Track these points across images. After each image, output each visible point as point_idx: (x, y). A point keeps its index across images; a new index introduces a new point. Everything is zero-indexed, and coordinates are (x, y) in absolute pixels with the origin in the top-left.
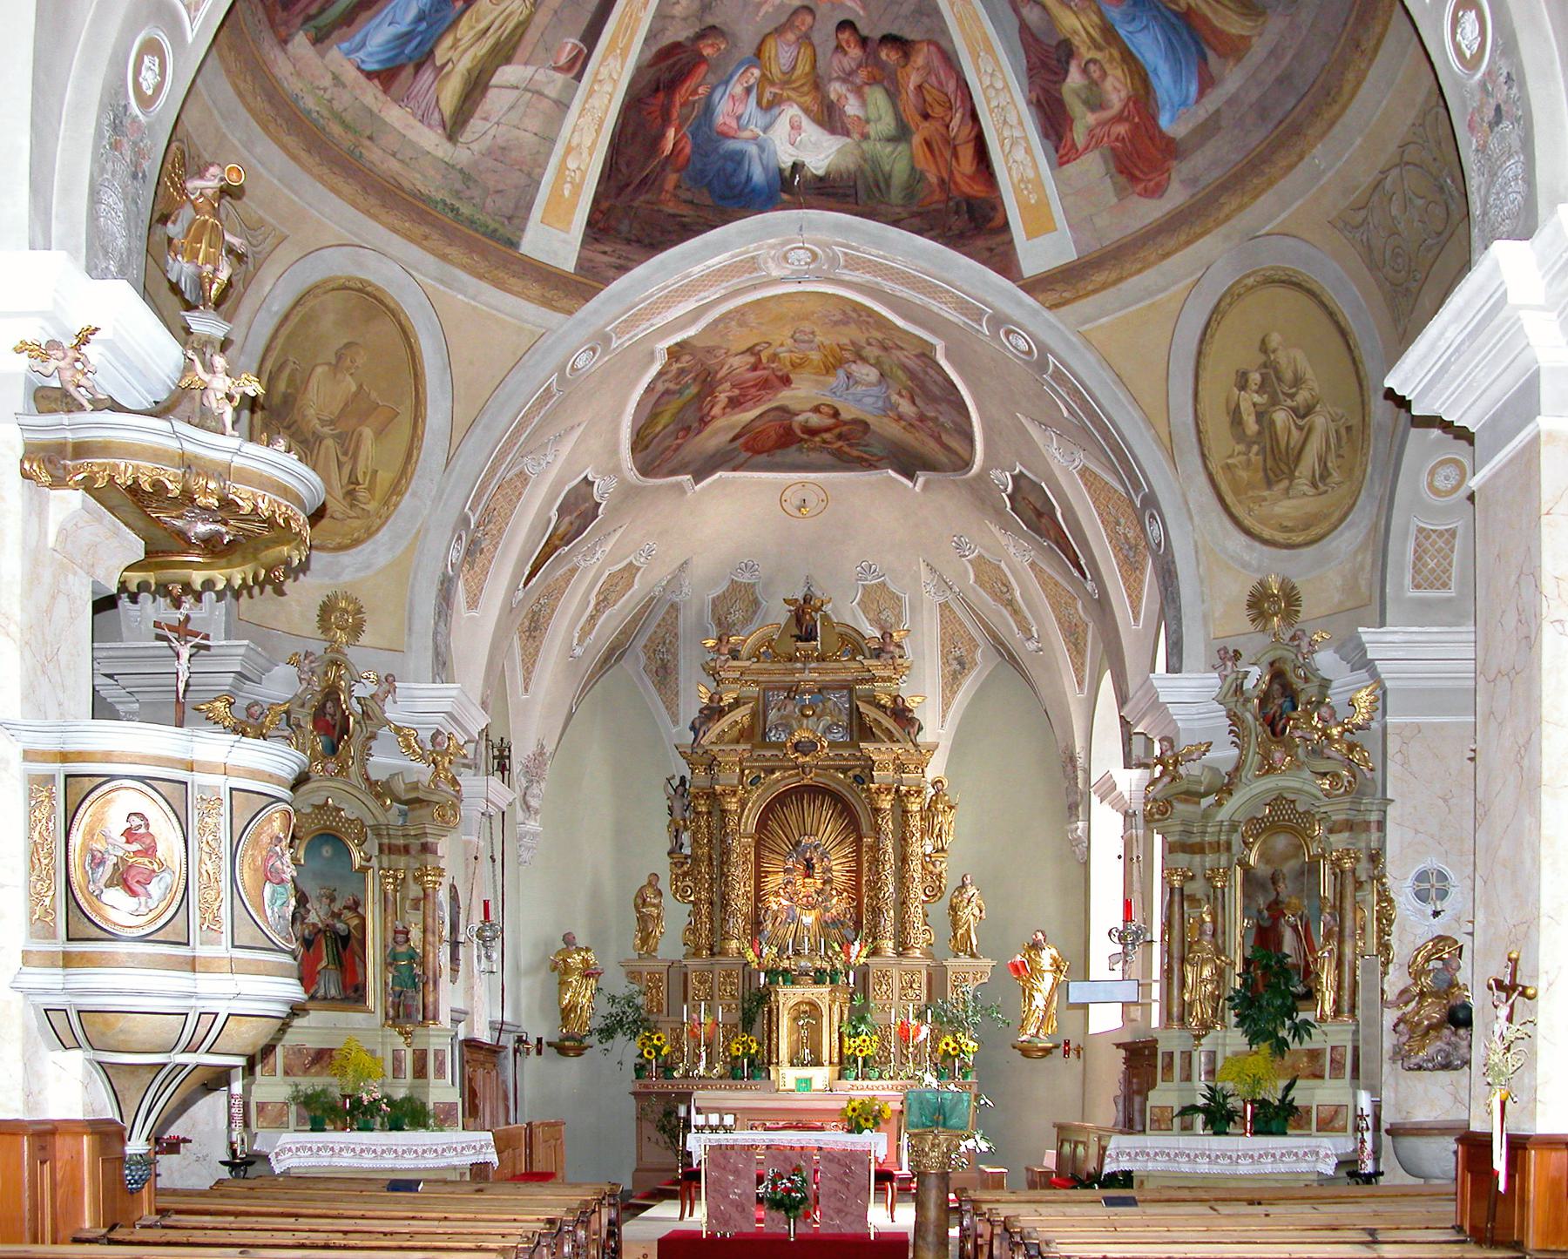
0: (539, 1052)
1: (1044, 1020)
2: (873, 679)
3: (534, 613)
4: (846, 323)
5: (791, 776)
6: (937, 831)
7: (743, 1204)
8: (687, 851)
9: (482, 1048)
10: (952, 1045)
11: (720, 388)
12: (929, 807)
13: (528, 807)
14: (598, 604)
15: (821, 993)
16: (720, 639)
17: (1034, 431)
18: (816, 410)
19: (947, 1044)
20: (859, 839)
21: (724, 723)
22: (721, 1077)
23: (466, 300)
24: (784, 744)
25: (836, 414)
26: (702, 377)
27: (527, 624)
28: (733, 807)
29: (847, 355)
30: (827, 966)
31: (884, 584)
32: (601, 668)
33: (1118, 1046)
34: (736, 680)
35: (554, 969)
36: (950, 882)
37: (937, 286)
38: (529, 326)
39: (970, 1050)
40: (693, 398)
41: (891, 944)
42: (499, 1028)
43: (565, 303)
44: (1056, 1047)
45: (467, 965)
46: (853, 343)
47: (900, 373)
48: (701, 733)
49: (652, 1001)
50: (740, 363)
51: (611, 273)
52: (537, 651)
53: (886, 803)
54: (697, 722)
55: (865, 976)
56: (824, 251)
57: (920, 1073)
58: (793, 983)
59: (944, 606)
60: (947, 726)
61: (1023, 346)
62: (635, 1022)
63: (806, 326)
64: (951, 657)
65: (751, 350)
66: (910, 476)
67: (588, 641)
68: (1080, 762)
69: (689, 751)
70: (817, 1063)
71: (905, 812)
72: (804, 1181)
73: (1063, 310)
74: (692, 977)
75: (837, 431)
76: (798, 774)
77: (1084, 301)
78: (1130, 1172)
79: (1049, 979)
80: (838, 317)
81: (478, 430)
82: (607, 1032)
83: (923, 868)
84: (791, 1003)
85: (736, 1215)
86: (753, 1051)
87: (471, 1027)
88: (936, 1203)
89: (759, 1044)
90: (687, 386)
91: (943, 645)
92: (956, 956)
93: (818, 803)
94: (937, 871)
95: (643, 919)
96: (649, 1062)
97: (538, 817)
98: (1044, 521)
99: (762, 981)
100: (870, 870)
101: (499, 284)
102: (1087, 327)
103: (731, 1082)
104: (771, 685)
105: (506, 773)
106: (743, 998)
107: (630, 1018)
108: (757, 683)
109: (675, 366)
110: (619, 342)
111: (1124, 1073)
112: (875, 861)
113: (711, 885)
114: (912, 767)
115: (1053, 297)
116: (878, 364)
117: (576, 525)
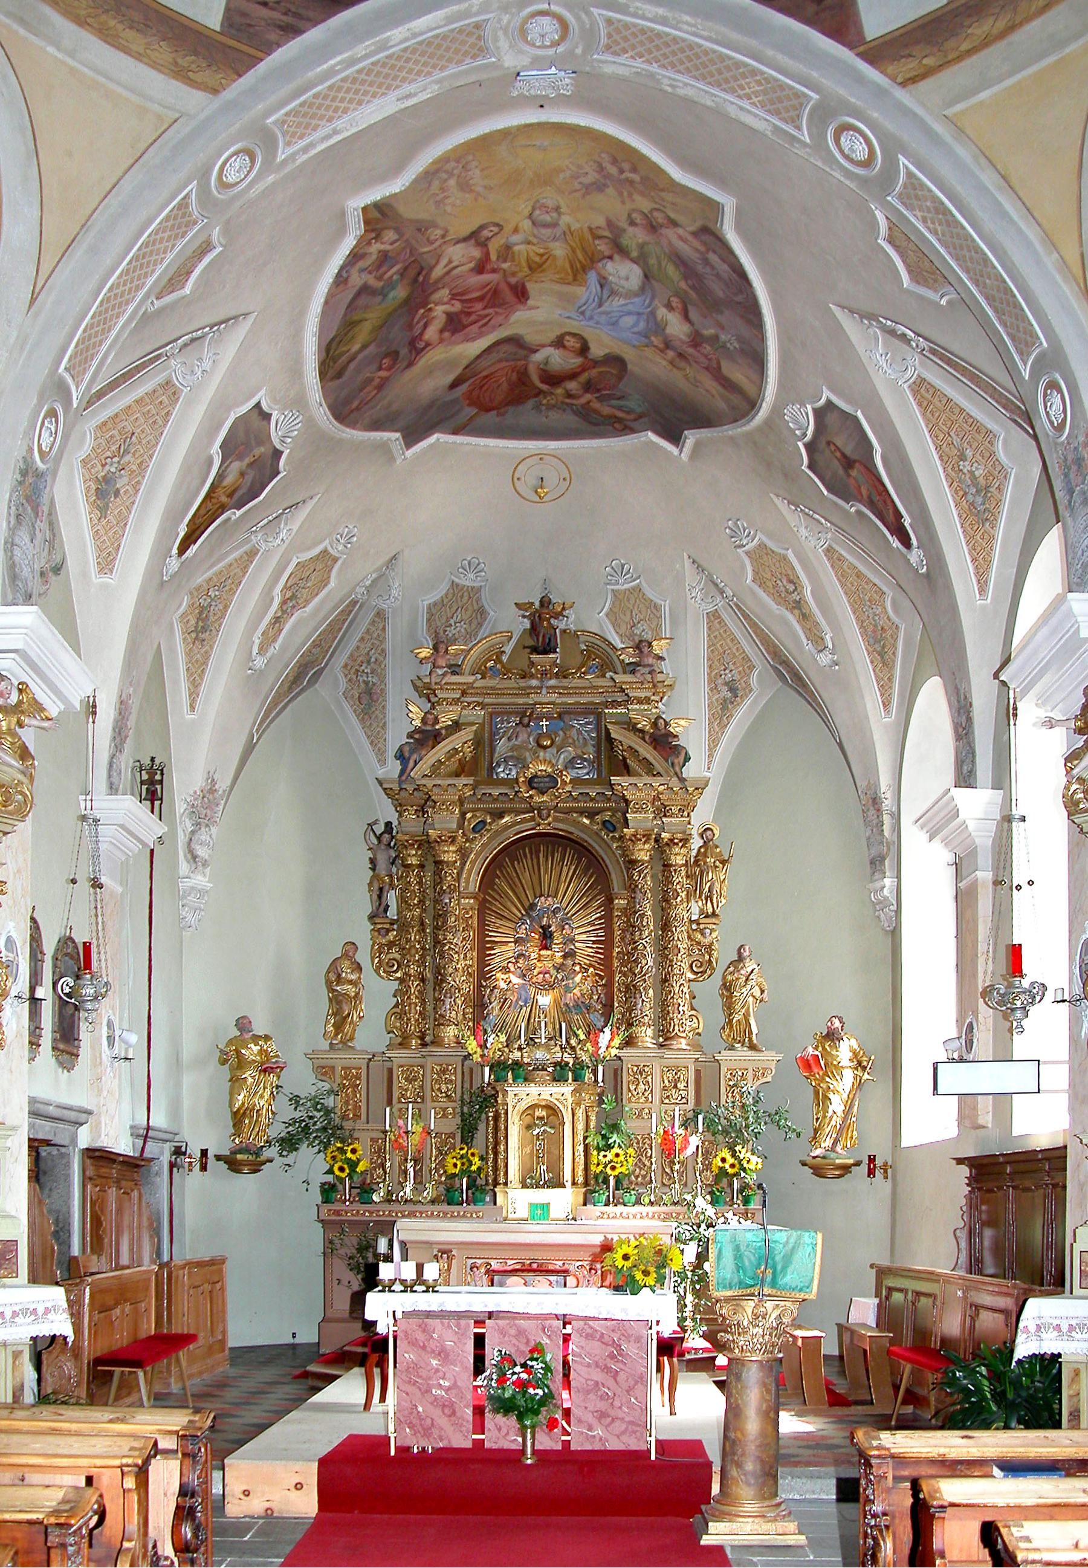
0: (204, 1168)
1: (842, 1129)
2: (628, 700)
3: (202, 609)
4: (600, 187)
5: (524, 821)
7: (452, 1403)
8: (392, 913)
9: (114, 1161)
10: (730, 1160)
11: (436, 296)
12: (696, 862)
13: (194, 857)
15: (562, 1093)
16: (436, 648)
17: (850, 326)
18: (559, 343)
19: (723, 1160)
20: (610, 900)
21: (440, 751)
22: (433, 1202)
23: (60, 56)
24: (516, 780)
25: (584, 349)
26: (412, 273)
27: (193, 622)
29: (603, 247)
30: (569, 1059)
31: (638, 589)
32: (290, 689)
33: (960, 1161)
34: (456, 701)
35: (223, 1062)
36: (723, 955)
37: (738, 64)
38: (156, 108)
39: (752, 1166)
40: (401, 306)
41: (650, 1032)
42: (146, 1134)
43: (205, 76)
44: (858, 1164)
45: (93, 1048)
46: (610, 224)
47: (671, 270)
49: (347, 1103)
50: (461, 255)
51: (273, 36)
52: (207, 656)
53: (643, 852)
54: (406, 749)
55: (617, 1074)
56: (578, 18)
57: (688, 1197)
58: (526, 1080)
59: (714, 617)
60: (714, 767)
61: (860, 152)
62: (324, 1129)
63: (550, 197)
64: (720, 681)
65: (474, 237)
66: (675, 438)
67: (271, 651)
68: (887, 804)
69: (396, 787)
70: (557, 1183)
71: (667, 866)
72: (547, 1368)
73: (923, 85)
74: (397, 1072)
75: (585, 377)
76: (533, 819)
77: (955, 68)
78: (1055, 1358)
79: (848, 1076)
80: (592, 176)
81: (79, 252)
82: (289, 1144)
83: (689, 937)
84: (523, 1105)
85: (443, 1421)
86: (474, 1168)
87: (96, 1131)
88: (759, 1410)
89: (482, 1158)
90: (391, 285)
91: (710, 667)
92: (732, 1048)
93: (557, 856)
94: (707, 941)
95: (337, 1000)
96: (342, 1181)
97: (208, 870)
98: (854, 473)
99: (486, 1080)
100: (623, 939)
101: (105, 35)
102: (958, 107)
103: (445, 1207)
104: (499, 709)
105: (157, 803)
106: (462, 1100)
107: (319, 1125)
108: (483, 706)
109: (375, 248)
110: (290, 150)
111: (969, 1198)
112: (632, 927)
113: (423, 956)
114: (675, 810)
115: (908, 67)
116: (641, 260)
117: (249, 478)
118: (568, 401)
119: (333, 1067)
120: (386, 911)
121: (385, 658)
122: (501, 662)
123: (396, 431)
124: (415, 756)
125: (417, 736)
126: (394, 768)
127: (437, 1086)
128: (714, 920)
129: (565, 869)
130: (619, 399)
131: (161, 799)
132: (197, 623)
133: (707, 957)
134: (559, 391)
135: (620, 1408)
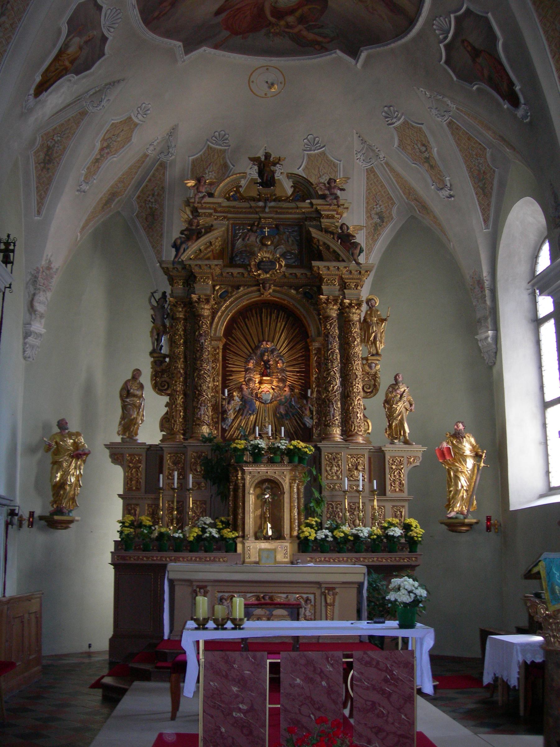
3: (49, 148)
6: (372, 338)
14: (102, 149)
28: (206, 313)
36: (385, 382)
48: (182, 250)
52: (50, 180)
59: (370, 171)
64: (373, 212)
66: (354, 53)
68: (487, 284)
70: (278, 535)
75: (298, 13)
79: (470, 463)
91: (367, 203)
92: (392, 443)
93: (274, 316)
94: (373, 371)
97: (43, 321)
98: (480, 60)
118: (287, 30)
119: (122, 454)
120: (161, 349)
121: (163, 192)
122: (239, 192)
123: (179, 41)
124: (184, 246)
125: (186, 233)
126: (170, 254)
127: (194, 467)
128: (378, 358)
129: (279, 324)
130: (319, 28)
131: (12, 263)
132: (45, 157)
133: (373, 381)
134: (282, 23)
135: (393, 724)
